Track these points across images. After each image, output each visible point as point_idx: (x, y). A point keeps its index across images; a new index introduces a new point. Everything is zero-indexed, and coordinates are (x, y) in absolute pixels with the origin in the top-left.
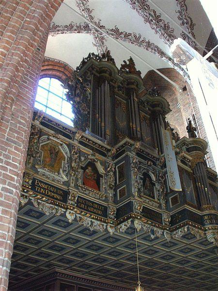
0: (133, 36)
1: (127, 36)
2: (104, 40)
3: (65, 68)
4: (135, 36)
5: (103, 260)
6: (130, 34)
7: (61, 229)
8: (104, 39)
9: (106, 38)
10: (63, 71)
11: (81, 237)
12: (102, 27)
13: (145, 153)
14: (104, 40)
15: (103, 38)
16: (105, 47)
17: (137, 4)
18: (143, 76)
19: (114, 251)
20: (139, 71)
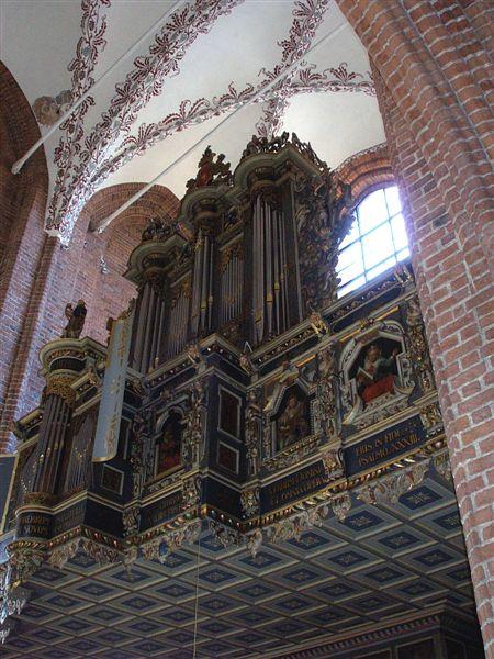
0: (300, 18)
1: (297, 29)
2: (312, 72)
3: (355, 169)
4: (301, 14)
5: (182, 591)
6: (296, 22)
7: (424, 510)
8: (308, 71)
9: (308, 66)
10: (356, 176)
11: (377, 532)
12: (277, 71)
13: (230, 357)
14: (312, 72)
15: (305, 74)
16: (328, 73)
17: (207, 12)
18: (232, 169)
19: (217, 571)
20: (257, 145)
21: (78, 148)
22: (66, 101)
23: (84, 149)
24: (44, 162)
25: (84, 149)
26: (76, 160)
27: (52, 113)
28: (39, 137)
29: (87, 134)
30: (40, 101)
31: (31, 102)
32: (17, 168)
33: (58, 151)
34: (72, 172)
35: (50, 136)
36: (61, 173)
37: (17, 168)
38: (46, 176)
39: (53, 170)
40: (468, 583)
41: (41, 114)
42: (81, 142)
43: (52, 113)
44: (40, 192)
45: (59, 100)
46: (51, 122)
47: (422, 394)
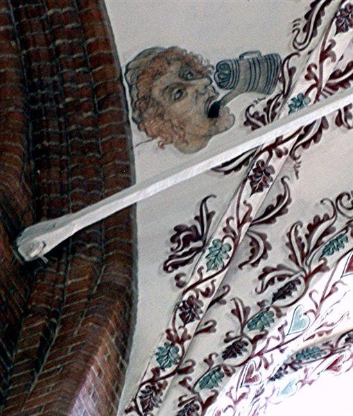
15: (123, 340)
21: (258, 249)
22: (251, 87)
23: (277, 256)
24: (129, 258)
25: (277, 256)
26: (246, 287)
27: (190, 108)
28: (125, 179)
29: (300, 213)
30: (156, 61)
31: (126, 49)
32: (42, 240)
33: (188, 240)
34: (225, 322)
35: (164, 183)
36: (188, 310)
37: (42, 240)
38: (125, 298)
39: (155, 298)
40: (35, 133)
41: (147, 99)
42: (276, 233)
43: (190, 108)
44: (108, 342)
45: (227, 74)
46: (186, 140)
47: (167, 338)
